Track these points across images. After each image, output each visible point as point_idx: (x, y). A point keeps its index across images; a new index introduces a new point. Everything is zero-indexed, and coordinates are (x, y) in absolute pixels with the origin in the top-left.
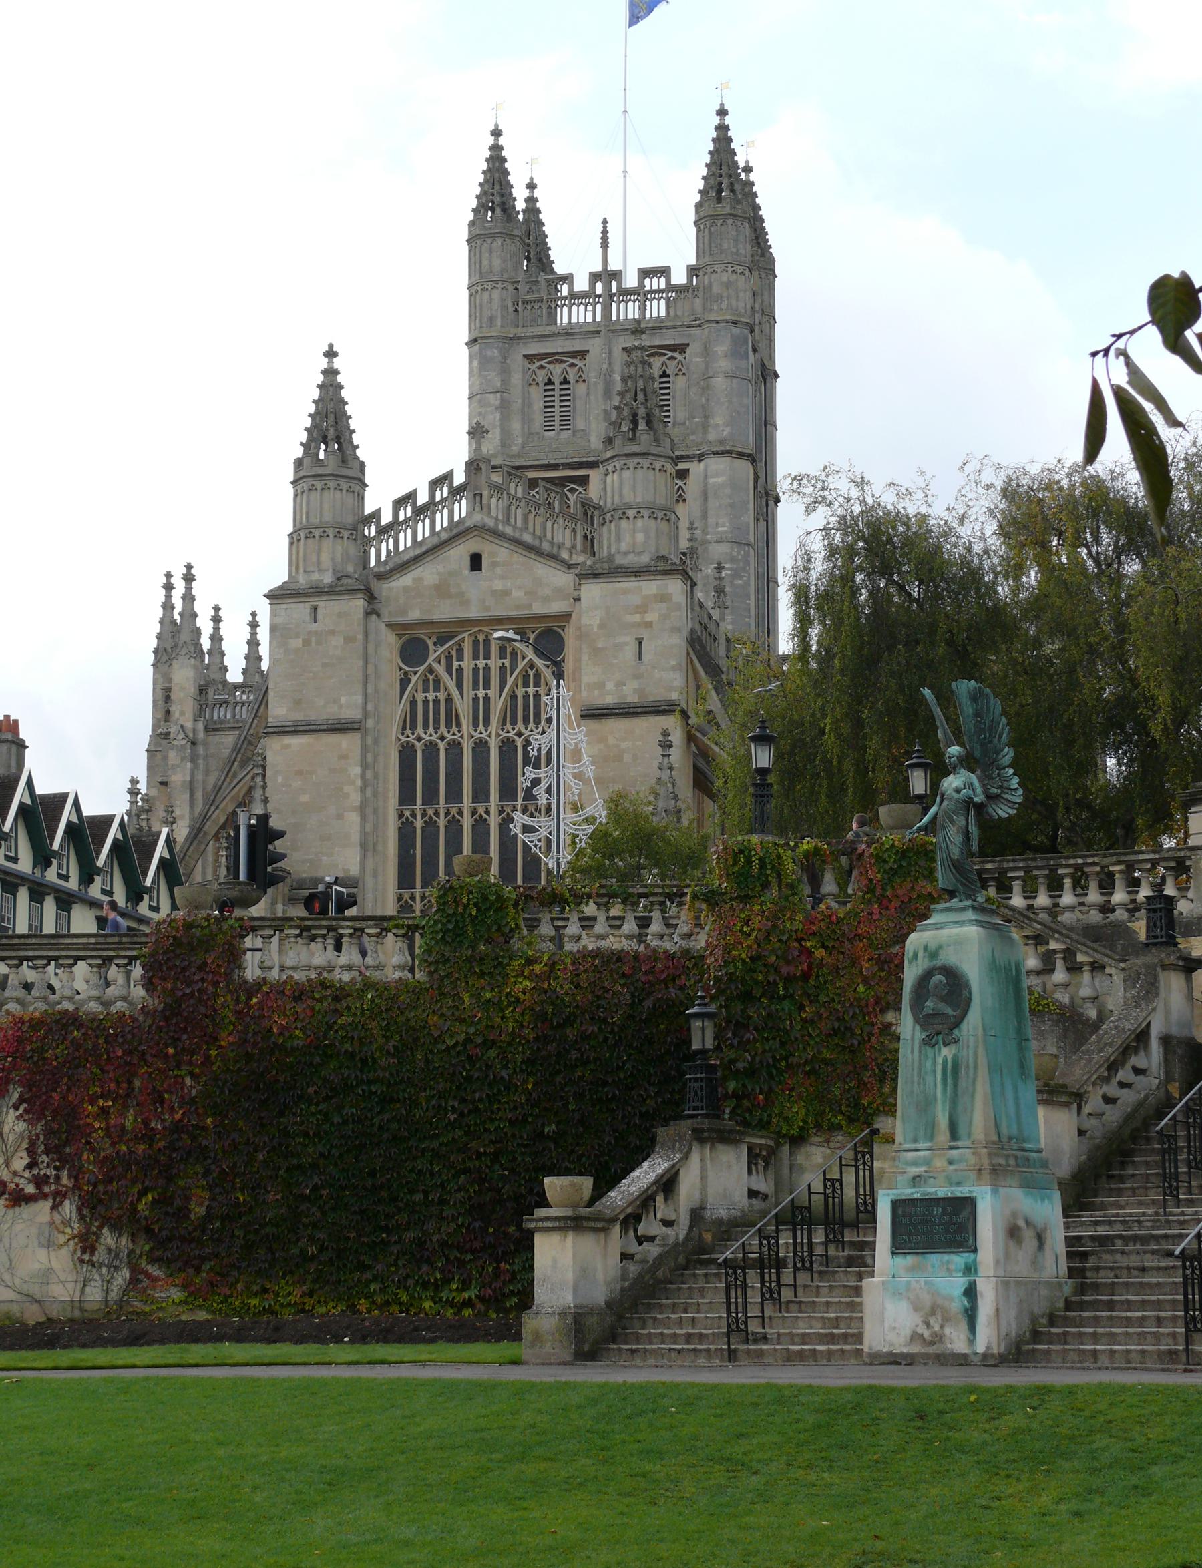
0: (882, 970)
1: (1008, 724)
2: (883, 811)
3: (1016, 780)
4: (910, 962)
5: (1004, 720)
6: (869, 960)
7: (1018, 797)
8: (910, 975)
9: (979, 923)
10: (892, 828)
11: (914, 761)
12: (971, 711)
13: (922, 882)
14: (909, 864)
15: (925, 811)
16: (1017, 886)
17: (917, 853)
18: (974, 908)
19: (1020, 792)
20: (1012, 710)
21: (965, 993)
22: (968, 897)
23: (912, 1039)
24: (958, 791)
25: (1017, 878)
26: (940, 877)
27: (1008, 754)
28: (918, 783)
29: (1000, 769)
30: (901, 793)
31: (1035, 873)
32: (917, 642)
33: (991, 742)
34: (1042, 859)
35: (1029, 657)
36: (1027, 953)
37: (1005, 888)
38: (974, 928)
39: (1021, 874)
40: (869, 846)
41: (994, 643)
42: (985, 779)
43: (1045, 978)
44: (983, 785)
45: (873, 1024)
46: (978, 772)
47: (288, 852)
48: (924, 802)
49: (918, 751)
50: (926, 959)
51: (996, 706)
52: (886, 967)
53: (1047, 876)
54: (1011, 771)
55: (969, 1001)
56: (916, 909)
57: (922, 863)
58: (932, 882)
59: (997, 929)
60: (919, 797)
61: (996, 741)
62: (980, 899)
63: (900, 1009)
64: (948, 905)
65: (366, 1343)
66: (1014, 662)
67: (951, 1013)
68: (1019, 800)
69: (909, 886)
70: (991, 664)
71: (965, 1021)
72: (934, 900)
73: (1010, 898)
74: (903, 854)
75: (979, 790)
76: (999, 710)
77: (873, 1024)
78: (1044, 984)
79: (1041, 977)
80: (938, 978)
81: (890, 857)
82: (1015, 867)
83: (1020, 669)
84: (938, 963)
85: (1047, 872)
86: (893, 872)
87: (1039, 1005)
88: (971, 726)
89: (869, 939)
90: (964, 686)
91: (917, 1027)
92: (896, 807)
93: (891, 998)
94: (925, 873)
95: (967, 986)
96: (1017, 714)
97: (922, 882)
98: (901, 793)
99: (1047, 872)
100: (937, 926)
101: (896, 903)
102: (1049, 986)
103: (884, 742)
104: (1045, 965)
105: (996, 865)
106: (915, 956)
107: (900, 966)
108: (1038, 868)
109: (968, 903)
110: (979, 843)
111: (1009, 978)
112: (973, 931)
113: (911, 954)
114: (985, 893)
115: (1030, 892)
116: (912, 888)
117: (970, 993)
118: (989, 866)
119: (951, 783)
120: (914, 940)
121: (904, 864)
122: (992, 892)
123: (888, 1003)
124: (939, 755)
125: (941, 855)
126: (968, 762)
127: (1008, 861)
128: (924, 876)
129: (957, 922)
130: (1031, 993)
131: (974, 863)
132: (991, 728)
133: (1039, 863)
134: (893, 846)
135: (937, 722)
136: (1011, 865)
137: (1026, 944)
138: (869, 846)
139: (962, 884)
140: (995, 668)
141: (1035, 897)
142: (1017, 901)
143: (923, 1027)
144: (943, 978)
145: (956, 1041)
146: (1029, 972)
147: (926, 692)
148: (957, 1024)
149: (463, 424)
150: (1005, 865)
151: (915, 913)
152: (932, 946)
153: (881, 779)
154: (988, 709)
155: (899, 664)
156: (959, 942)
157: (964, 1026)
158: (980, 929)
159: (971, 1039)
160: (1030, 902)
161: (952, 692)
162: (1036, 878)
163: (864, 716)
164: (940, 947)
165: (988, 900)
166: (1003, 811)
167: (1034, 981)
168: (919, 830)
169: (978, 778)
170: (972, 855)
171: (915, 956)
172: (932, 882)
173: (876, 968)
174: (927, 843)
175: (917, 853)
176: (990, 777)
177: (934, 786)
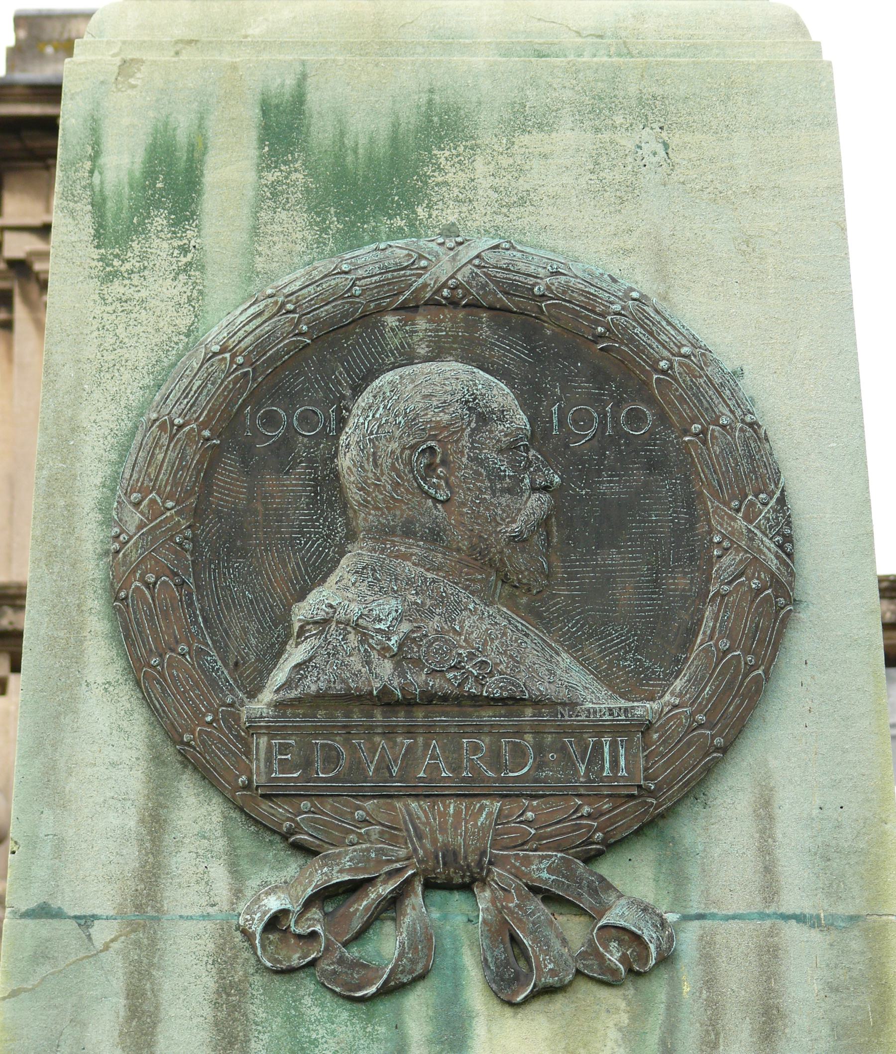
23: (144, 910)
50: (292, 229)
55: (773, 605)
65: (261, 142)
71: (731, 801)
80: (428, 385)
91: (198, 813)
106: (173, 183)
143: (265, 815)
145: (636, 961)
148: (650, 812)
149: (855, 310)
152: (358, 109)
157: (722, 830)
159: (807, 962)
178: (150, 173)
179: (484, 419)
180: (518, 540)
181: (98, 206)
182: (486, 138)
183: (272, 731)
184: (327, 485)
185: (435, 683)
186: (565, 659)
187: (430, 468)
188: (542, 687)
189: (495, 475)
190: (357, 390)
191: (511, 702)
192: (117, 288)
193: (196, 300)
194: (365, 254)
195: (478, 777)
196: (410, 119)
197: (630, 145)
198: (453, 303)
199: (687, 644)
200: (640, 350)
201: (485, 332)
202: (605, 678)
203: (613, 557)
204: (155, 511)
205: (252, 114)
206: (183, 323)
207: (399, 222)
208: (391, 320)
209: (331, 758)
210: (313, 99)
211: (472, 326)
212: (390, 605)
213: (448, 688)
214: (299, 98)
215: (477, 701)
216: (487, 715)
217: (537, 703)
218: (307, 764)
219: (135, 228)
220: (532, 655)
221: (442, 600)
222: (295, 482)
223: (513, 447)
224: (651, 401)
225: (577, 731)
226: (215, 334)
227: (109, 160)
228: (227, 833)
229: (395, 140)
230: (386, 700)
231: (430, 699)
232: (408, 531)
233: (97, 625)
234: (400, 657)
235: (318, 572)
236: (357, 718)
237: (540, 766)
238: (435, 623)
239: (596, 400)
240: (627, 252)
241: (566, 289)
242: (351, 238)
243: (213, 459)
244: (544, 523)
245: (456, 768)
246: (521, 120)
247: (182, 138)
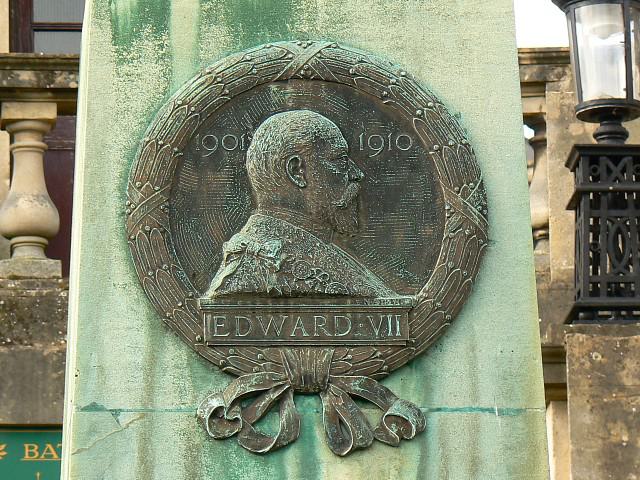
50: (219, 33)
55: (478, 244)
80: (283, 127)
180: (342, 209)
183: (213, 312)
184: (240, 178)
187: (296, 170)
191: (340, 296)
192: (125, 68)
193: (168, 75)
198: (306, 78)
199: (431, 265)
203: (391, 217)
208: (274, 87)
209: (244, 326)
211: (316, 90)
215: (322, 296)
216: (327, 304)
217: (353, 297)
218: (232, 329)
219: (136, 35)
225: (375, 312)
226: (178, 94)
231: (296, 295)
235: (237, 225)
236: (259, 305)
237: (355, 330)
239: (383, 132)
241: (367, 71)
242: (250, 40)
243: (179, 163)
244: (356, 199)
245: (311, 331)
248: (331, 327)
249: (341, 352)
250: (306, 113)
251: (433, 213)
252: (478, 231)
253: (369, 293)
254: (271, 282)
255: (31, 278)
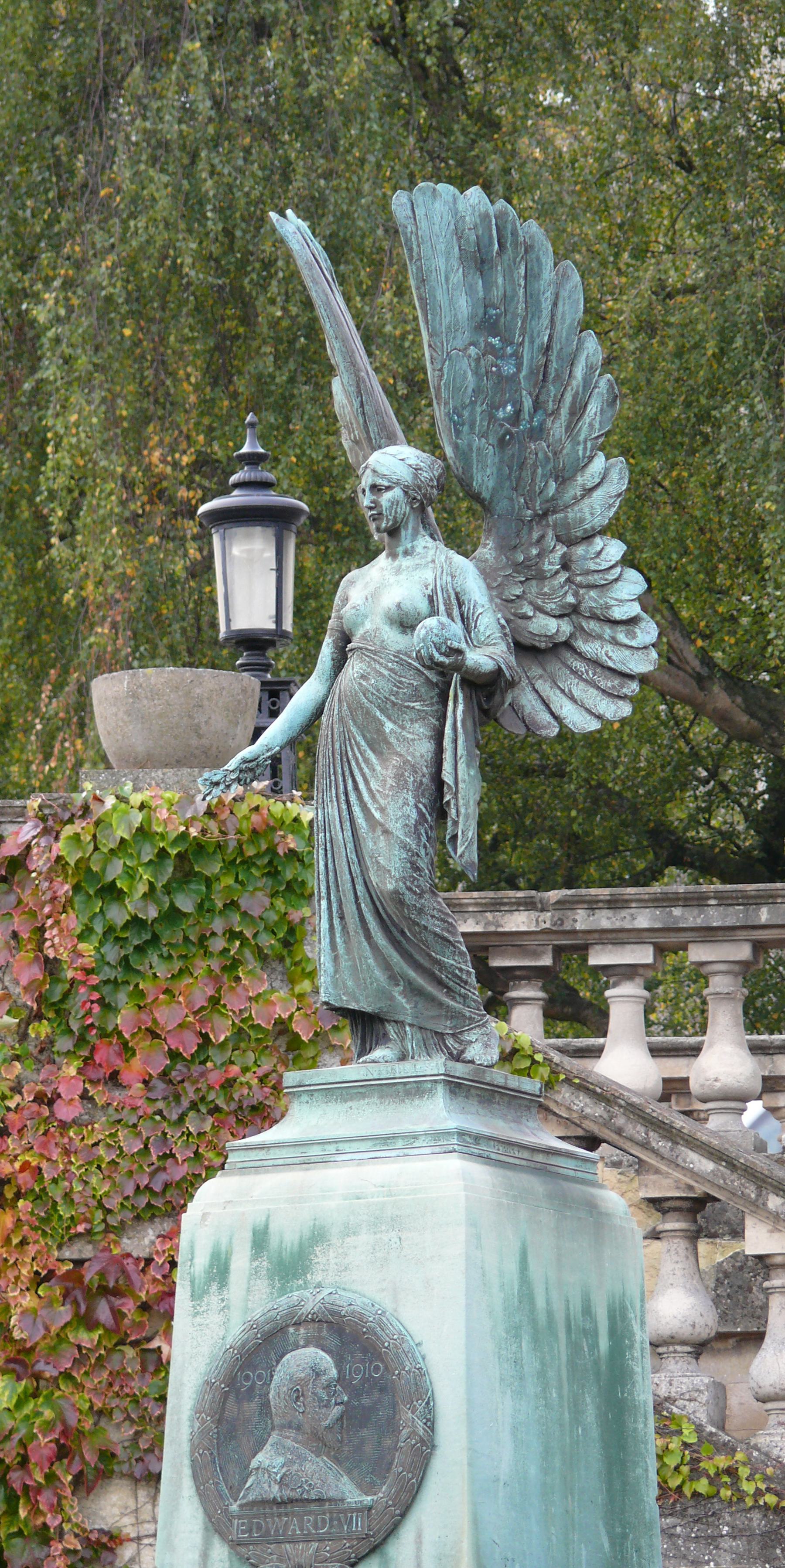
0: (88, 1322)
1: (608, 362)
2: (107, 691)
3: (633, 584)
4: (197, 1296)
5: (592, 348)
6: (38, 1280)
7: (638, 651)
8: (197, 1344)
9: (472, 1144)
10: (143, 762)
11: (236, 499)
12: (464, 306)
13: (254, 980)
14: (204, 908)
15: (275, 696)
16: (624, 1004)
17: (239, 863)
18: (455, 1087)
19: (648, 632)
20: (624, 309)
21: (410, 1419)
22: (434, 1041)
24: (405, 623)
25: (629, 972)
26: (325, 961)
27: (603, 484)
28: (250, 584)
29: (571, 543)
30: (177, 624)
31: (697, 953)
32: (261, 30)
33: (538, 433)
34: (724, 900)
35: (695, 102)
36: (655, 1270)
37: (576, 1011)
38: (454, 1165)
39: (644, 955)
40: (50, 832)
41: (565, 43)
42: (516, 574)
43: (721, 1366)
44: (507, 604)
45: (44, 1536)
46: (487, 551)
47: (249, 1228)
48: (267, 660)
49: (253, 460)
50: (262, 1286)
51: (563, 290)
52: (103, 1312)
53: (744, 970)
54: (615, 550)
55: (424, 1452)
56: (229, 1084)
57: (256, 901)
58: (291, 981)
59: (543, 1171)
60: (253, 643)
61: (557, 428)
62: (482, 1050)
63: (154, 1479)
64: (354, 1072)
66: (639, 119)
67: (352, 1494)
68: (644, 664)
69: (201, 993)
70: (550, 127)
72: (291, 1046)
73: (596, 1052)
74: (187, 860)
75: (488, 622)
76: (573, 309)
77: (44, 1536)
78: (720, 1391)
79: (708, 1362)
80: (306, 1358)
81: (130, 874)
82: (621, 925)
83: (659, 144)
84: (308, 1298)
85: (744, 952)
86: (142, 936)
87: (696, 1473)
88: (465, 366)
89: (39, 1197)
90: (439, 208)
92: (160, 677)
93: (118, 1435)
94: (267, 941)
95: (420, 1393)
96: (647, 327)
97: (254, 980)
98: (177, 624)
99: (744, 952)
100: (309, 1154)
101: (148, 1060)
102: (739, 1400)
103: (112, 421)
104: (723, 1317)
105: (547, 920)
106: (219, 1270)
107: (159, 1309)
108: (709, 934)
109: (433, 1065)
110: (482, 825)
111: (587, 1363)
112: (453, 1179)
113: (202, 1261)
114: (496, 1026)
115: (675, 1034)
116: (215, 1001)
117: (431, 1424)
118: (518, 922)
119: (378, 591)
120: (219, 1211)
121: (185, 903)
122: (526, 1023)
123: (107, 1455)
124: (330, 478)
125: (332, 871)
126: (450, 509)
127: (592, 905)
128: (261, 956)
129: (386, 1140)
130: (667, 1426)
131: (457, 907)
132: (542, 376)
133: (715, 916)
134: (143, 832)
135: (334, 352)
136: (605, 920)
137: (655, 1235)
138: (50, 832)
139: (414, 991)
140: (563, 142)
141: (695, 1051)
142: (625, 1062)
144: (326, 1361)
146: (660, 1345)
147: (292, 227)
150: (581, 920)
151: (223, 1101)
152: (287, 1232)
153: (96, 563)
154: (532, 300)
155: (188, 113)
156: (391, 1219)
158: (480, 1172)
160: (675, 1067)
161: (393, 231)
162: (700, 974)
163: (41, 314)
164: (318, 1236)
165: (509, 1056)
166: (575, 706)
167: (682, 1381)
168: (249, 772)
169: (486, 574)
170: (453, 878)
171: (219, 1270)
172: (291, 981)
173: (65, 1313)
174: (270, 828)
175: (239, 863)
176: (532, 571)
177: (312, 601)
178: (211, 1266)
179: (318, 1375)
180: (329, 1428)
181: (192, 1282)
182: (334, 1241)
183: (240, 1517)
184: (265, 1405)
185: (292, 1494)
186: (345, 1479)
187: (298, 1398)
188: (332, 1494)
189: (321, 1400)
190: (278, 1362)
191: (320, 1501)
192: (198, 1319)
193: (226, 1323)
194: (283, 1300)
195: (310, 1534)
196: (307, 1233)
197: (386, 1239)
198: (313, 1320)
199: (389, 1470)
200: (378, 1338)
201: (325, 1333)
202: (359, 1486)
203: (365, 1433)
204: (203, 1422)
205: (249, 1235)
206: (221, 1334)
207: (301, 1282)
208: (291, 1330)
209: (259, 1527)
210: (272, 1227)
211: (320, 1330)
212: (281, 1460)
213: (298, 1496)
214: (267, 1227)
215: (309, 1501)
216: (313, 1507)
217: (330, 1500)
218: (250, 1531)
219: (206, 1292)
220: (331, 1479)
221: (299, 1457)
222: (252, 1406)
223: (329, 1386)
224: (382, 1361)
225: (344, 1511)
226: (230, 1340)
227: (197, 1261)
228: (231, 1561)
229: (301, 1244)
230: (274, 1501)
231: (291, 1501)
232: (290, 1427)
233: (187, 1472)
234: (281, 1483)
235: (259, 1446)
236: (268, 1510)
237: (331, 1527)
238: (296, 1467)
239: (362, 1361)
240: (383, 1290)
241: (353, 1312)
242: (283, 1291)
243: (226, 1395)
244: (340, 1418)
245: (302, 1530)
246: (349, 1231)
247: (223, 1249)
248: (316, 1527)
249: (322, 1545)
250: (311, 1351)
251: (392, 1426)
252: (422, 1441)
253: (340, 1496)
254: (275, 1491)
255: (561, 1407)
